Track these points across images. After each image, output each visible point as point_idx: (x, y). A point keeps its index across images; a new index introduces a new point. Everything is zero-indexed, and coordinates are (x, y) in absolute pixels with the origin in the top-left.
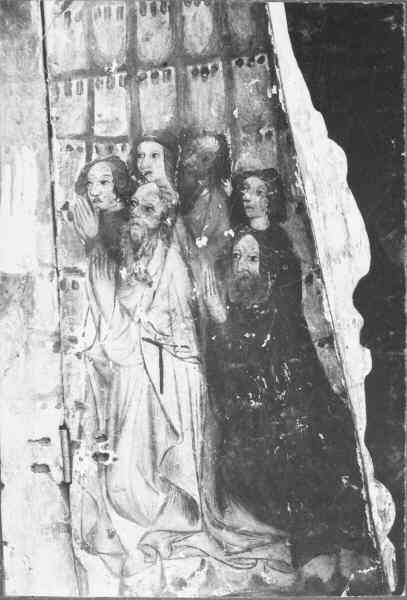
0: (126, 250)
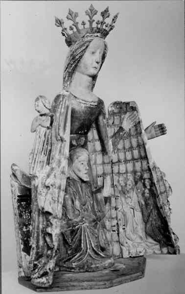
0: (126, 192)
